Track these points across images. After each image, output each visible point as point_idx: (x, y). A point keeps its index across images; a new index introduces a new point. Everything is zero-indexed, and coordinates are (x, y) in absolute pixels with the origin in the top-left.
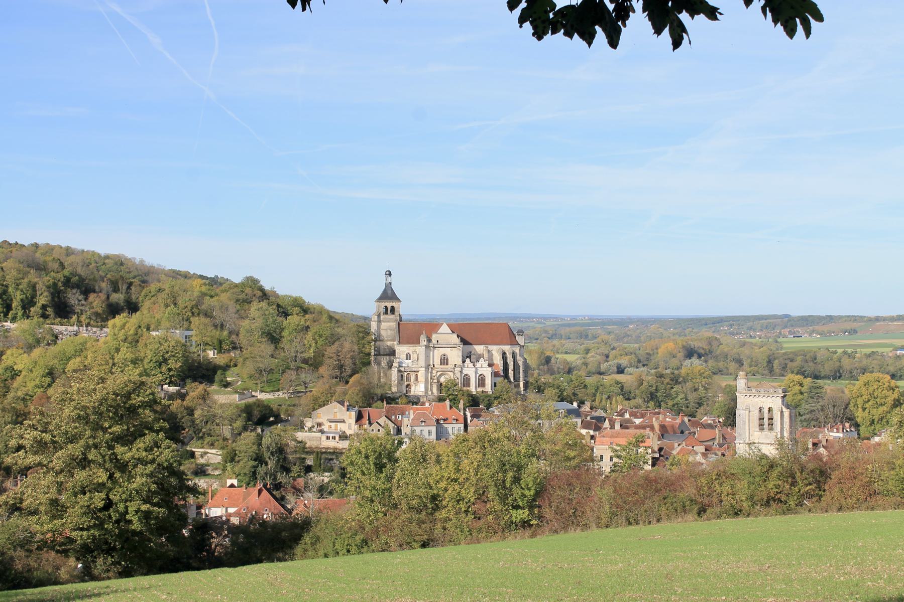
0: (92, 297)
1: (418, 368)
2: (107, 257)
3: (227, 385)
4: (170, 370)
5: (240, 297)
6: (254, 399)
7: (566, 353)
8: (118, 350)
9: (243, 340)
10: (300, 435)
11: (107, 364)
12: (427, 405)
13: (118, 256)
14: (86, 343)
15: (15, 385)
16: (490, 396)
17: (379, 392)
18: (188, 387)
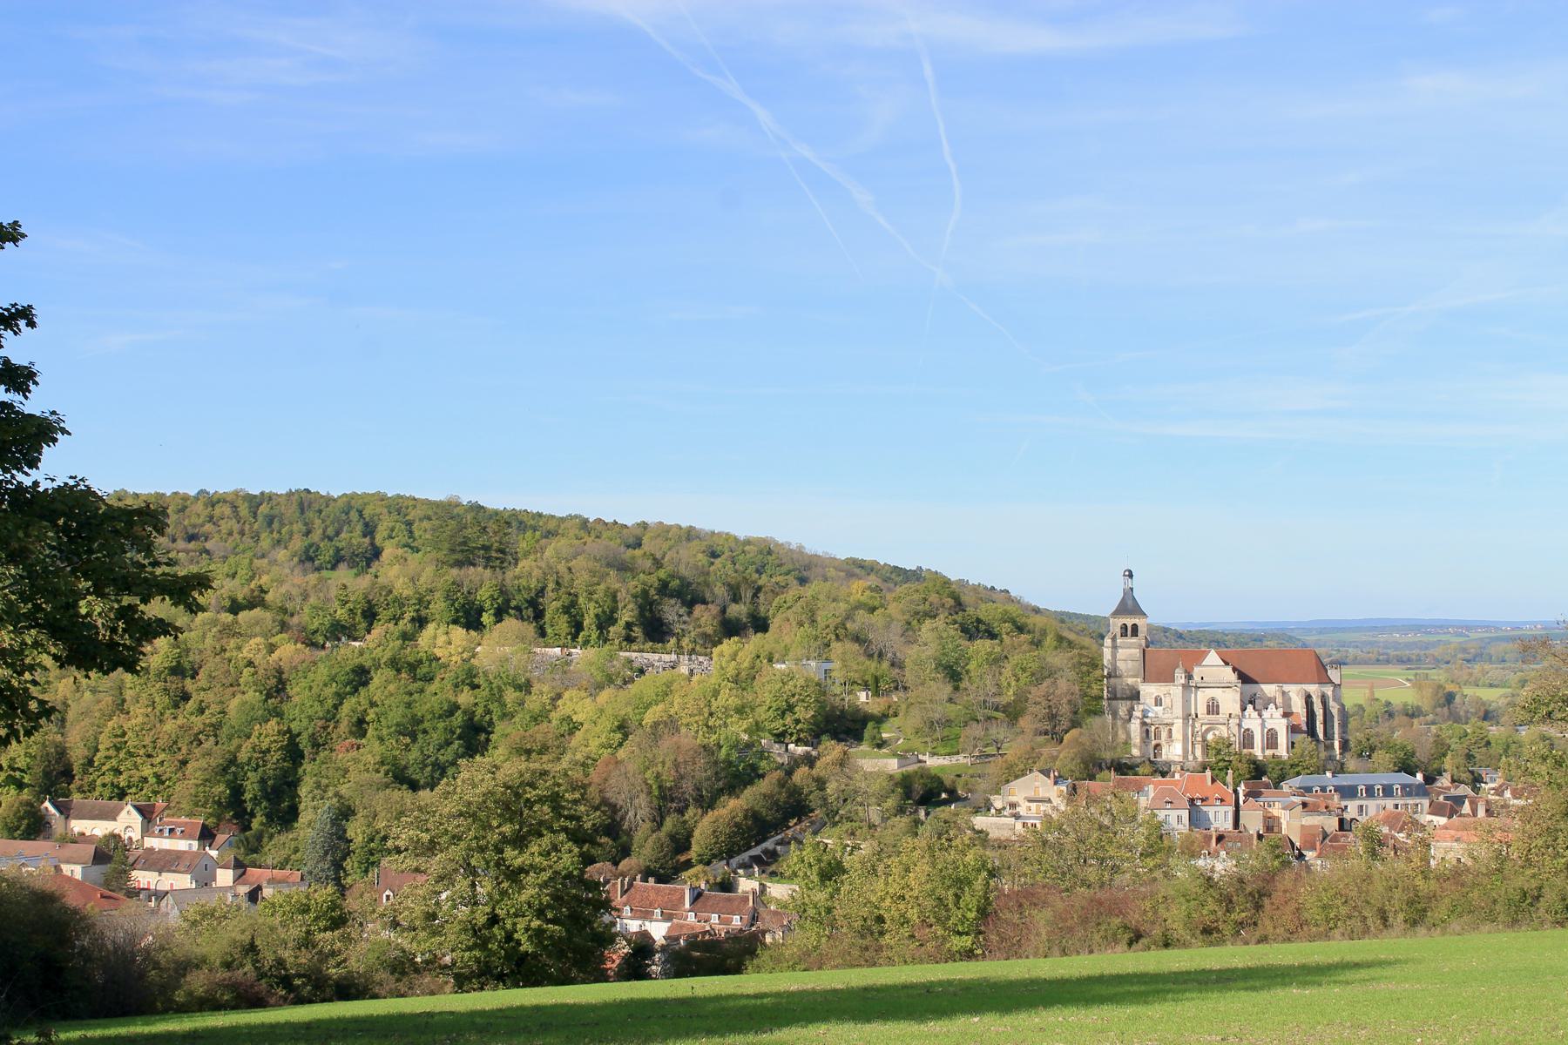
0: (698, 609)
1: (1179, 716)
2: (748, 542)
3: (881, 744)
4: (798, 721)
5: (921, 608)
6: (915, 767)
7: (1491, 686)
8: (716, 693)
9: (909, 677)
10: (980, 821)
11: (700, 713)
12: (1177, 776)
13: (764, 540)
14: (671, 683)
15: (574, 743)
16: (1284, 763)
17: (1108, 756)
18: (821, 748)
